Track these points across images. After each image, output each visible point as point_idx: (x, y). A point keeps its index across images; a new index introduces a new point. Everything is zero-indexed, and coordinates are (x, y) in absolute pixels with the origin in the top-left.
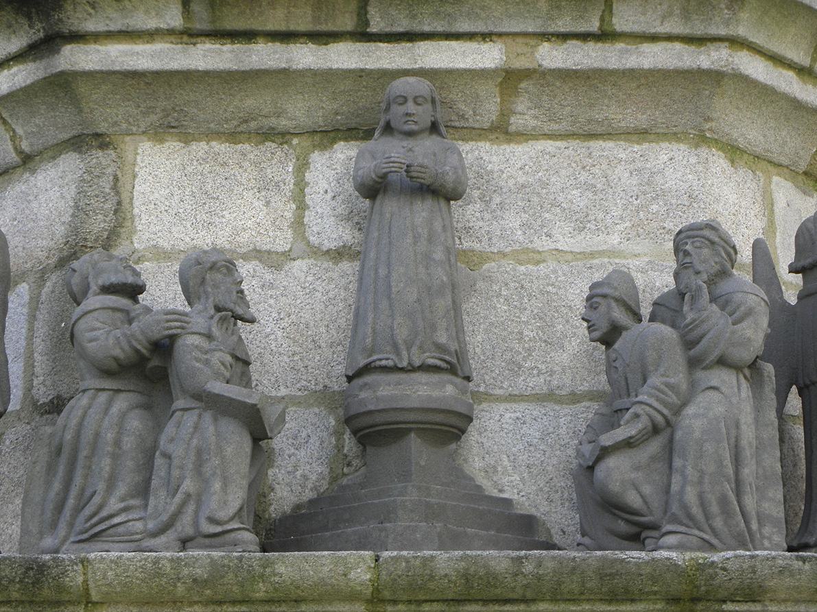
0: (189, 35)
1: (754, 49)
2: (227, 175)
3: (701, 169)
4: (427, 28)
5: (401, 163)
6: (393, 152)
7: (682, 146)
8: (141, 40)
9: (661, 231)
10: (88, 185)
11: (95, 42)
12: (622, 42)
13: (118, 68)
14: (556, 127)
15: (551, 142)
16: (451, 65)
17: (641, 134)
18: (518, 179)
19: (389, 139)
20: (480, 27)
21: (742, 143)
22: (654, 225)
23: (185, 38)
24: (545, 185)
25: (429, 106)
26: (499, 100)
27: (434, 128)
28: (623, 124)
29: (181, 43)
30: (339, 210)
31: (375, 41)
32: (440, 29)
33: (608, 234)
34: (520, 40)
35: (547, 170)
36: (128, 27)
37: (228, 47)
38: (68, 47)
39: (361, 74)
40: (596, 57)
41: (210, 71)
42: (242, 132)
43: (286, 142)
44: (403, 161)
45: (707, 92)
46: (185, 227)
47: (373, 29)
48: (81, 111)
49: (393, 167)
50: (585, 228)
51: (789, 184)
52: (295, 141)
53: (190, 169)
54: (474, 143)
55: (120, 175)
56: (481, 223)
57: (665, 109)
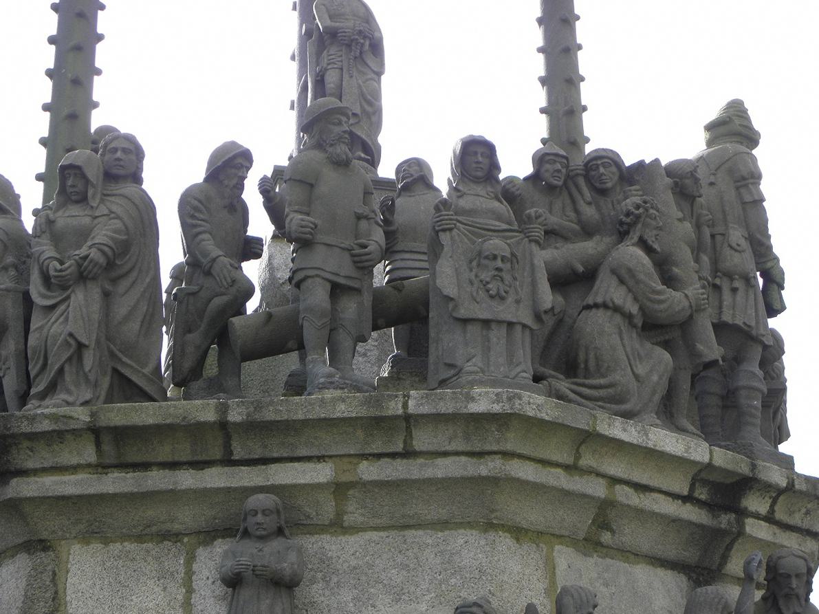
0: (102, 467)
1: (524, 457)
2: (135, 568)
3: (488, 549)
4: (275, 455)
5: (247, 565)
6: (249, 553)
7: (474, 532)
8: (68, 473)
9: (458, 599)
10: (35, 578)
11: (35, 475)
12: (422, 458)
13: (51, 494)
14: (379, 521)
15: (375, 533)
16: (294, 481)
17: (443, 524)
18: (351, 563)
19: (247, 541)
20: (315, 452)
21: (524, 525)
22: (453, 594)
23: (100, 470)
24: (370, 566)
25: (275, 516)
26: (334, 503)
27: (280, 532)
28: (429, 517)
29: (97, 474)
30: (217, 592)
31: (238, 466)
32: (285, 455)
33: (418, 603)
34: (346, 460)
35: (373, 555)
36: (57, 464)
37: (130, 475)
38: (15, 480)
39: (228, 490)
40: (403, 470)
41: (118, 494)
42: (146, 534)
43: (179, 541)
44: (249, 563)
45: (489, 492)
46: (103, 609)
47: (236, 457)
48: (28, 524)
49: (242, 568)
50: (400, 599)
51: (570, 550)
52: (186, 540)
53: (108, 564)
54: (318, 536)
55: (57, 571)
56: (323, 599)
57: (459, 505)
